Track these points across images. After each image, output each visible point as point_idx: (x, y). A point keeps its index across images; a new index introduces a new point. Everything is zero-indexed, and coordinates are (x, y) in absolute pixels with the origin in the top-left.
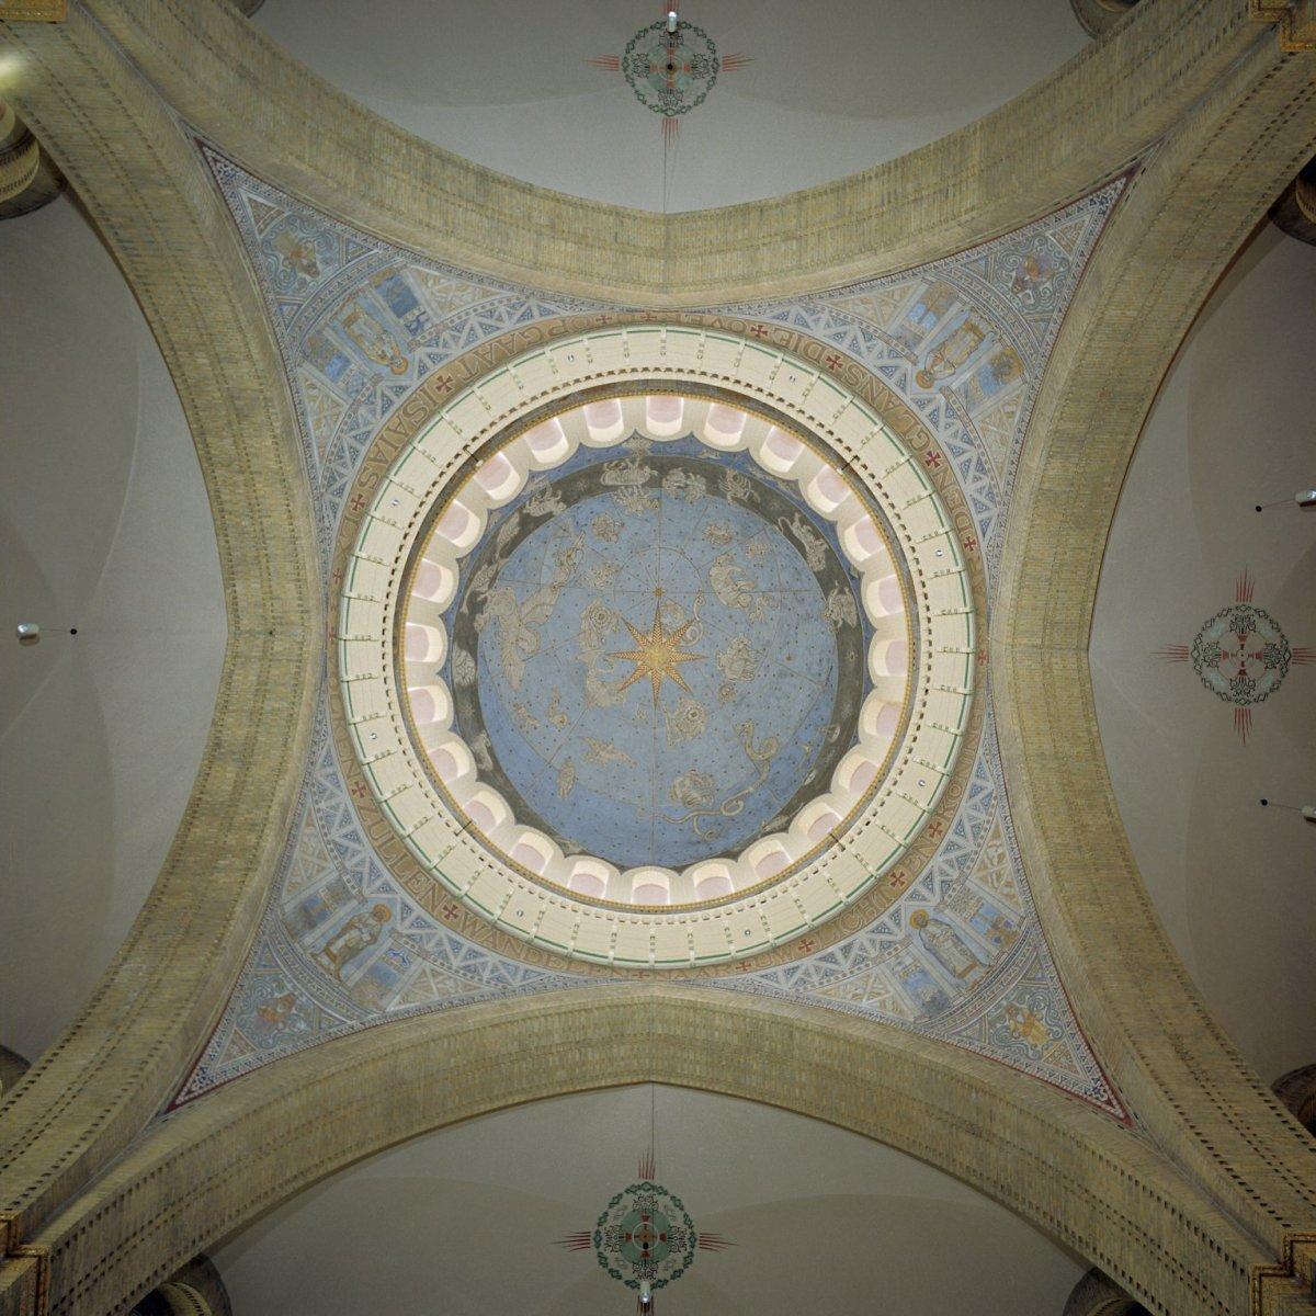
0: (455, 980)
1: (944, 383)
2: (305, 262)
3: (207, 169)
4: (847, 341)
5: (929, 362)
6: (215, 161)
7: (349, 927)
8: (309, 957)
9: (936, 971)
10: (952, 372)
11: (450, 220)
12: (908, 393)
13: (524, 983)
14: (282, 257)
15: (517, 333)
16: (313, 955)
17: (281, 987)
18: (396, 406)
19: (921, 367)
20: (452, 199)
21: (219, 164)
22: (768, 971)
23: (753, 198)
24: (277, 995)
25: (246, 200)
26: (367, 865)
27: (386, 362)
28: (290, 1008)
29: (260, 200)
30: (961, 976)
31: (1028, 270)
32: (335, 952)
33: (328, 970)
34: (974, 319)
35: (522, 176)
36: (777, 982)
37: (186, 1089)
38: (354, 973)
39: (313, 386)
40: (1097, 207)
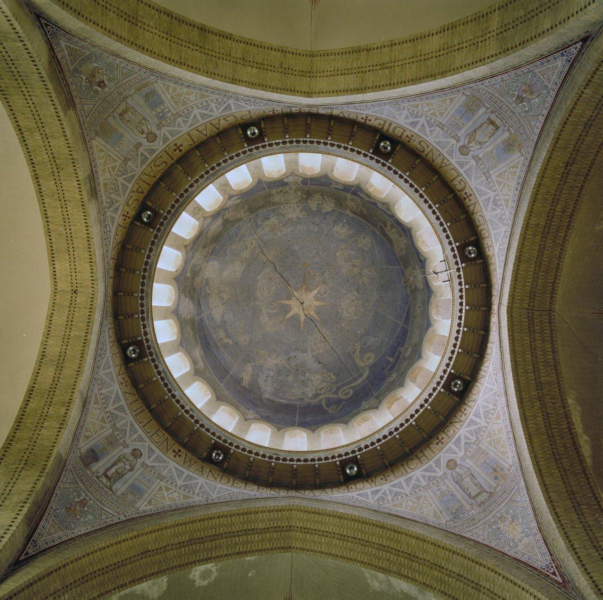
0: (179, 493)
1: (476, 153)
2: (98, 80)
3: (42, 30)
4: (419, 126)
5: (466, 141)
6: (47, 25)
7: (119, 460)
8: (95, 478)
9: (459, 495)
10: (480, 147)
11: (183, 56)
12: (454, 157)
13: (219, 495)
14: (84, 78)
15: (221, 118)
16: (97, 477)
17: (79, 495)
18: (150, 160)
19: (461, 143)
20: (184, 44)
21: (48, 27)
22: (363, 491)
23: (363, 43)
24: (76, 500)
25: (64, 47)
26: (129, 425)
27: (144, 136)
28: (84, 507)
29: (72, 46)
30: (474, 498)
31: (525, 91)
32: (110, 476)
33: (106, 486)
34: (493, 117)
35: (226, 28)
36: (367, 498)
37: (25, 552)
38: (120, 487)
39: (101, 150)
40: (565, 58)
